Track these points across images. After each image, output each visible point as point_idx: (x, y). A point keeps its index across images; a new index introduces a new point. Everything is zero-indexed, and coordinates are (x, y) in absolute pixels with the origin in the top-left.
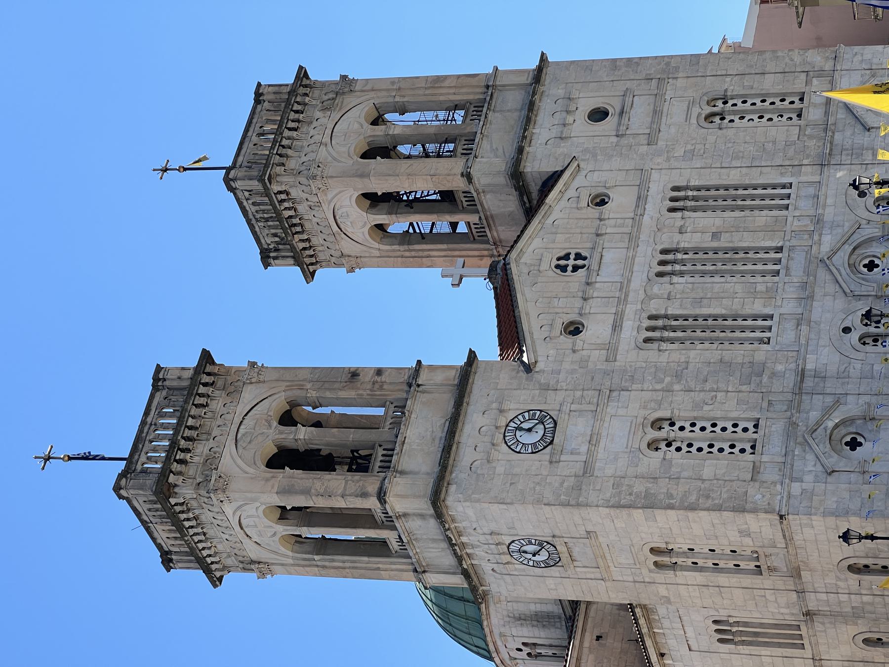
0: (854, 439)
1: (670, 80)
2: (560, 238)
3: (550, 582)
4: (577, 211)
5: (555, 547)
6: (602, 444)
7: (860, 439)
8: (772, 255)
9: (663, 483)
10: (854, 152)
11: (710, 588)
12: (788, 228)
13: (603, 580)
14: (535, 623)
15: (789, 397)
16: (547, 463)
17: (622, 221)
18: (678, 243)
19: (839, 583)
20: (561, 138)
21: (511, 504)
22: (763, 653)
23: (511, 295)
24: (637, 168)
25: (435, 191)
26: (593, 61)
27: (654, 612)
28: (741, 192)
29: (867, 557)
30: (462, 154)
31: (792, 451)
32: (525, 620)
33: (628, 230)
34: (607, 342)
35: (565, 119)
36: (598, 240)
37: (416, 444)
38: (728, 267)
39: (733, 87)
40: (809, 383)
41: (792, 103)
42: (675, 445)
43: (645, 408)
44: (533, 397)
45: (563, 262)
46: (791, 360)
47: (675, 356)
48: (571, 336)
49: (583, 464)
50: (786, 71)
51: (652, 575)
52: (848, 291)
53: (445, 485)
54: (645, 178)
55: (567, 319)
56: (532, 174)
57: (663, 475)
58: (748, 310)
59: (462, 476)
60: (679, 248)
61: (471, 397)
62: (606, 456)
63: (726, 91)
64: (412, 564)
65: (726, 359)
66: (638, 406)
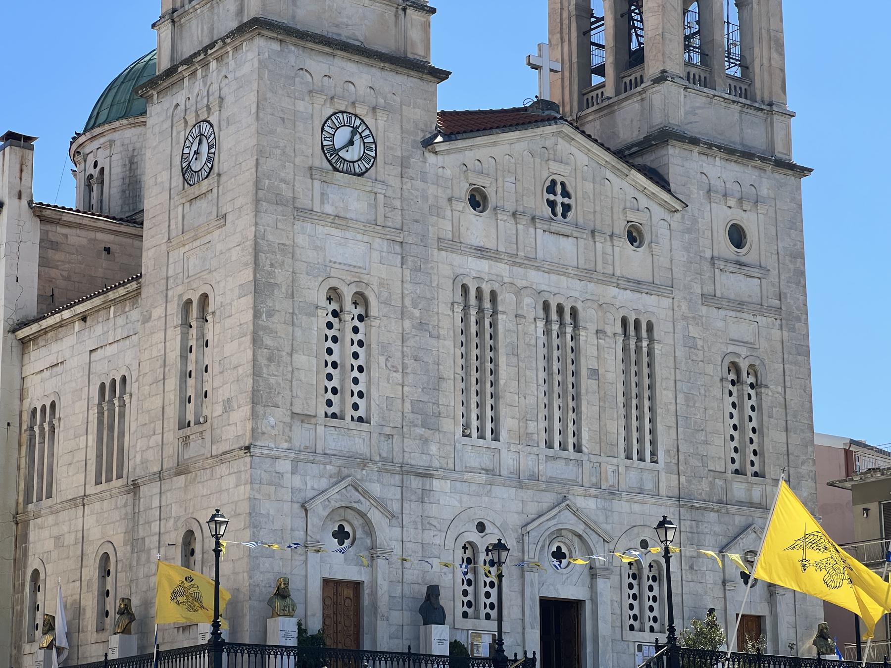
0: (347, 535)
1: (778, 321)
2: (589, 186)
3: (165, 176)
4: (622, 207)
5: (206, 178)
6: (334, 231)
7: (347, 542)
8: (571, 441)
9: (287, 305)
10: (694, 535)
11: (162, 369)
12: (604, 459)
13: (169, 239)
14: (127, 181)
15: (398, 459)
16: (310, 164)
17: (610, 262)
18: (585, 328)
19: (172, 521)
20: (709, 191)
21: (258, 118)
22: (90, 437)
23: (517, 125)
24: (674, 280)
25: (643, 44)
26: (802, 231)
27: (133, 306)
28: (647, 404)
29: (203, 553)
30: (689, 73)
31: (331, 462)
32: (130, 169)
33: (600, 267)
34: (462, 240)
35: (732, 196)
36: (586, 231)
37: (331, 4)
38: (557, 389)
39: (771, 394)
40: (415, 483)
41: (752, 464)
42: (335, 321)
43: (381, 285)
44: (392, 149)
45: (559, 189)
46: (443, 461)
47: (446, 323)
48: (468, 197)
49: (310, 207)
50: (790, 456)
51: (176, 299)
52: (529, 528)
53: (280, 37)
54: (662, 290)
55: (490, 192)
56: (665, 155)
57: (296, 305)
58: (503, 411)
59: (292, 59)
60: (579, 329)
61: (391, 73)
62: (320, 236)
63: (767, 387)
64: (183, 6)
65: (444, 385)
66: (383, 276)
